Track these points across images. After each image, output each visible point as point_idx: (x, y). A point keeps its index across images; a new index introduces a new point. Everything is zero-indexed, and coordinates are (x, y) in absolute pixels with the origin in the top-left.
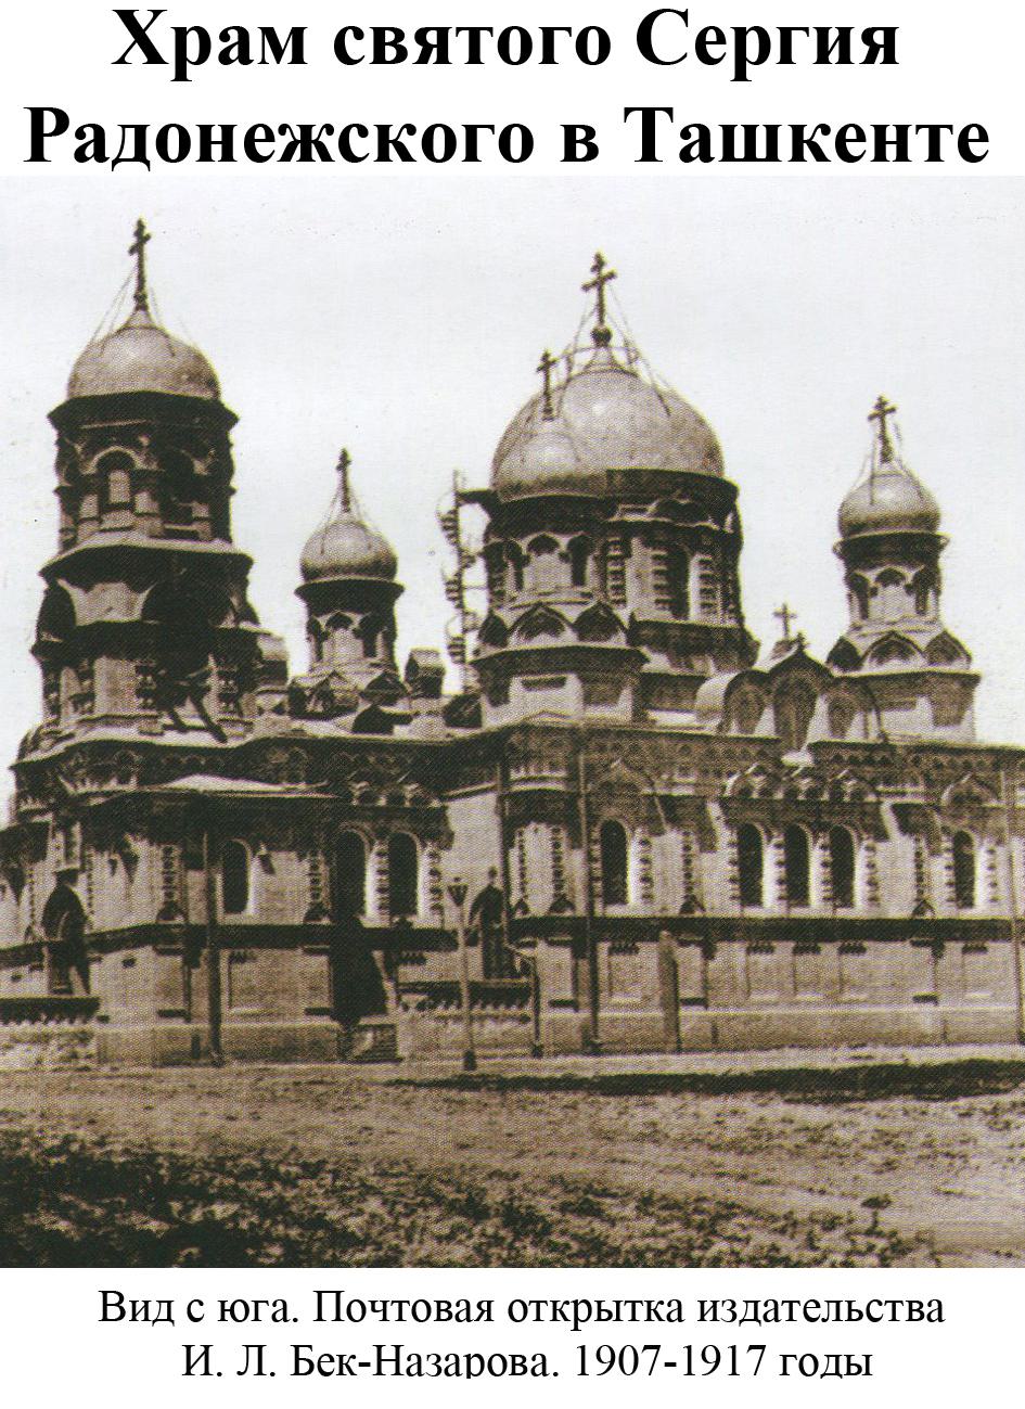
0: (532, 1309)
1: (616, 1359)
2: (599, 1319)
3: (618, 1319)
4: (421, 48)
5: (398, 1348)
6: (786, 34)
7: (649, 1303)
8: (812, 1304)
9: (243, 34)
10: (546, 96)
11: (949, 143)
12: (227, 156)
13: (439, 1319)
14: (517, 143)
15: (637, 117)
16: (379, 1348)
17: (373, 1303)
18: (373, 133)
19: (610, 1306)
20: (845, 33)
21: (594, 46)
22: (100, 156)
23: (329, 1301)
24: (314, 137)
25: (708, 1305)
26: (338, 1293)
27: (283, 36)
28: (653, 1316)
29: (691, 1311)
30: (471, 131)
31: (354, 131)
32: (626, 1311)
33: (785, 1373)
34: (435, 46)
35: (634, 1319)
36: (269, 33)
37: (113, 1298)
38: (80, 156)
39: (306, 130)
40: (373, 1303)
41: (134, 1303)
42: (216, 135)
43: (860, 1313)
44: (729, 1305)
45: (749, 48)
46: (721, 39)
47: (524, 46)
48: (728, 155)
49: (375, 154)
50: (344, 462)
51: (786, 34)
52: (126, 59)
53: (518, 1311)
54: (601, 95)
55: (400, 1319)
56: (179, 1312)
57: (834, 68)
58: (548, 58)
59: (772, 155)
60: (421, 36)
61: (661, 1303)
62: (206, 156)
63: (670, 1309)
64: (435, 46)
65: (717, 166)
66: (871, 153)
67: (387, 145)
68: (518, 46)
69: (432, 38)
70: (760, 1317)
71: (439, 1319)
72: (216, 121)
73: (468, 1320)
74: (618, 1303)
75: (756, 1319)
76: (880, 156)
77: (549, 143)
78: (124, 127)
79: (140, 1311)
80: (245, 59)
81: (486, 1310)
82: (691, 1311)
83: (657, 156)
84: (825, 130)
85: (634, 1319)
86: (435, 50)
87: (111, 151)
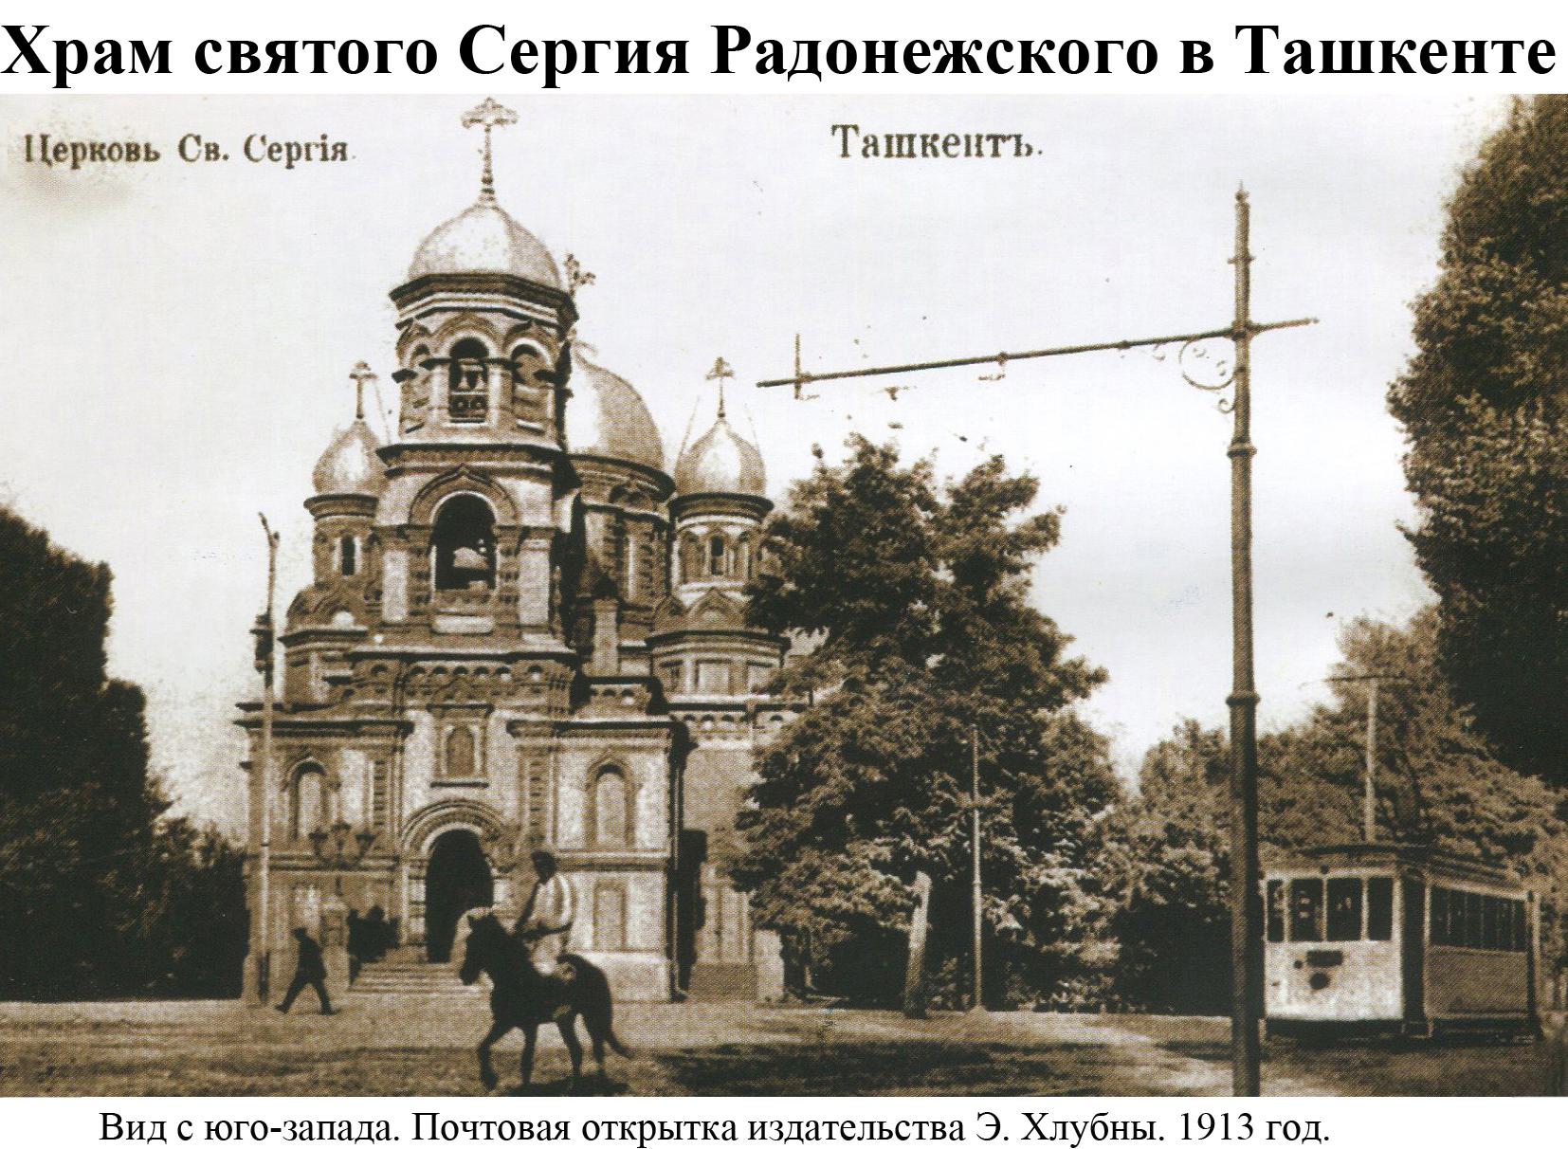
0: (604, 1129)
6: (590, 46)
9: (116, 47)
11: (1520, 57)
15: (1247, 34)
18: (1017, 49)
20: (642, 46)
22: (778, 68)
23: (426, 1122)
25: (757, 1126)
26: (434, 1115)
27: (151, 49)
29: (742, 1131)
31: (1000, 46)
32: (685, 1131)
34: (283, 57)
36: (138, 46)
37: (112, 1120)
38: (761, 68)
39: (957, 45)
46: (533, 51)
48: (1328, 67)
49: (1018, 67)
50: (1316, 321)
51: (590, 46)
53: (591, 1130)
56: (170, 1132)
57: (633, 76)
59: (1366, 67)
60: (271, 48)
64: (283, 57)
65: (1317, 75)
66: (1452, 64)
67: (1029, 58)
69: (281, 50)
72: (880, 37)
76: (1460, 68)
77: (1171, 57)
79: (136, 1131)
80: (117, 68)
81: (564, 1130)
82: (742, 1131)
84: (1412, 45)
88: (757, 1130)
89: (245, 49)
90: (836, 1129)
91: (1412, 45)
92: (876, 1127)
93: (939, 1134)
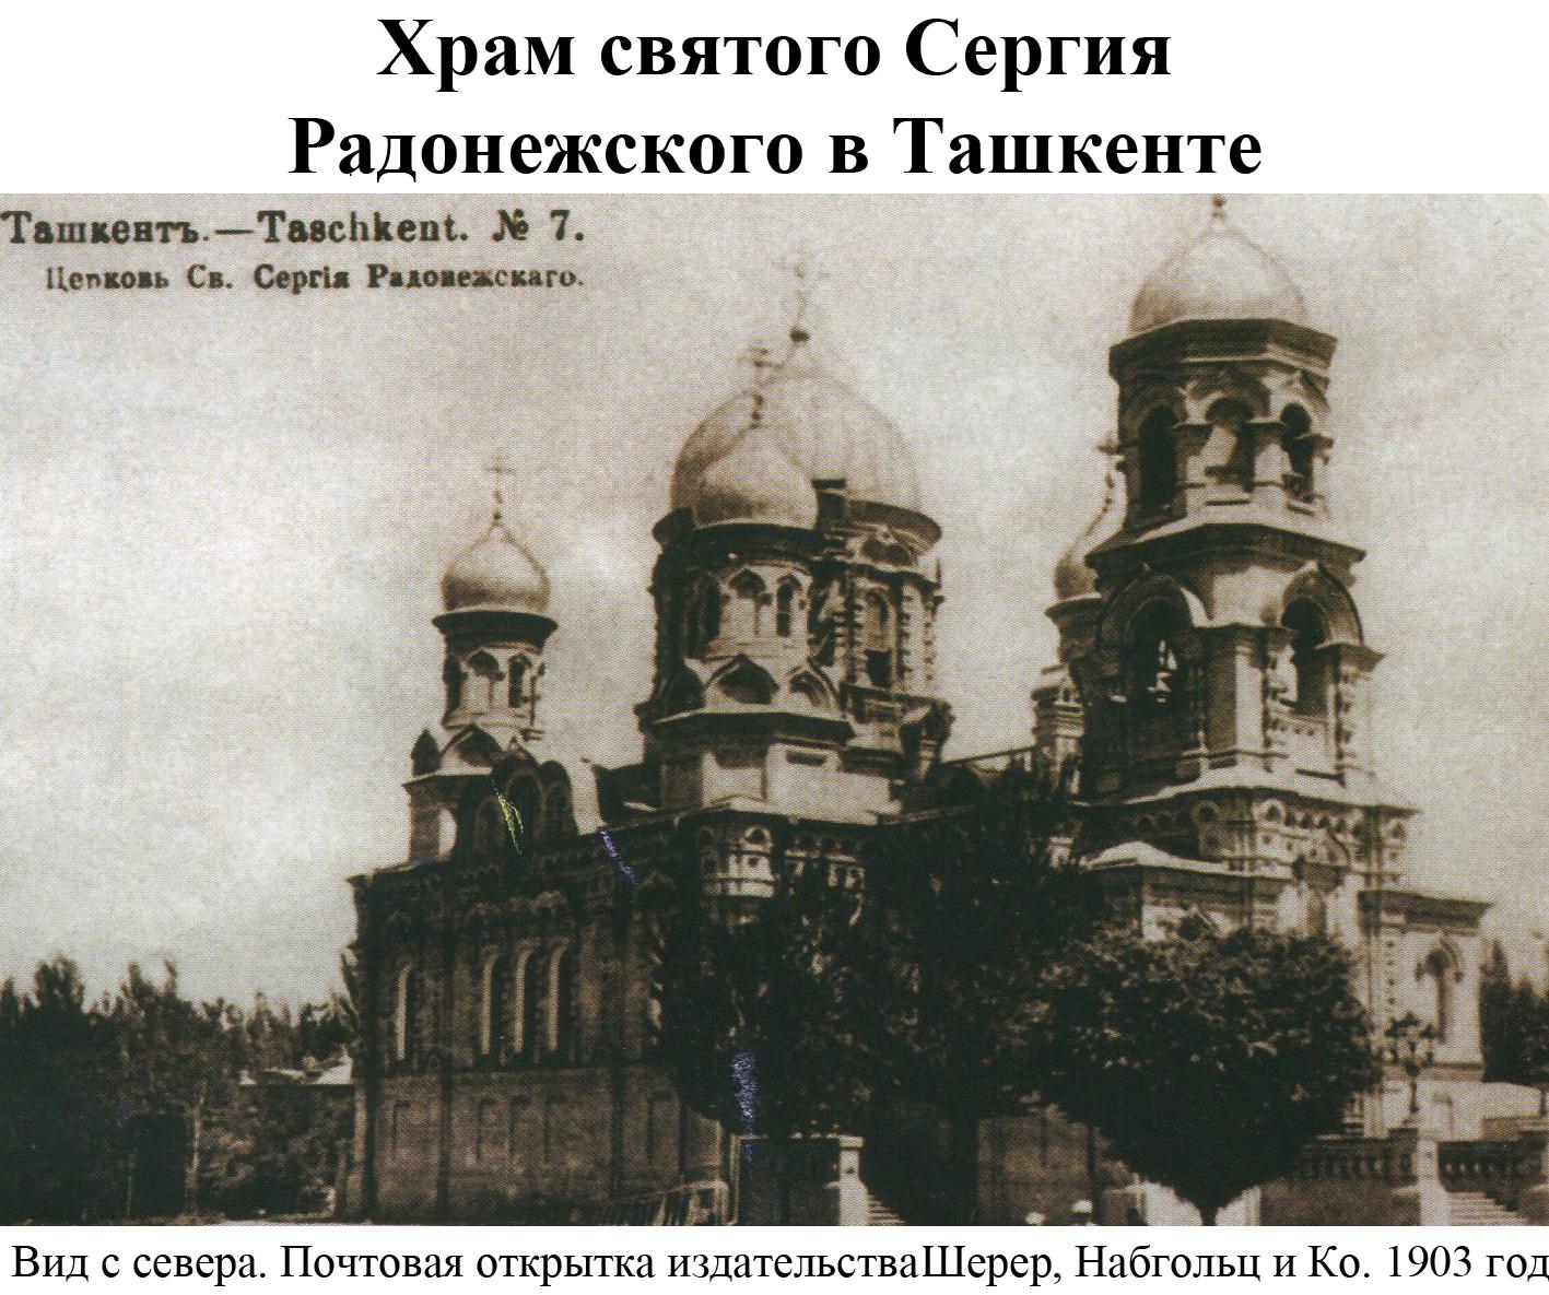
0: (502, 1265)
1: (1429, 1260)
2: (569, 1274)
3: (588, 1274)
4: (1139, 58)
5: (1100, 1249)
6: (1057, 44)
7: (619, 1258)
8: (784, 1259)
9: (510, 45)
10: (814, 107)
11: (1221, 154)
12: (494, 167)
13: (407, 1274)
14: (786, 154)
15: (906, 128)
16: (1082, 1249)
17: (341, 1258)
18: (641, 144)
19: (579, 1261)
20: (1116, 43)
21: (863, 56)
22: (365, 167)
23: (296, 1257)
24: (581, 148)
25: (678, 1261)
26: (306, 1249)
27: (550, 46)
28: (623, 1271)
29: (661, 1266)
30: (740, 142)
31: (621, 142)
32: (596, 1266)
33: (1492, 1274)
34: (702, 56)
35: (604, 1274)
37: (26, 1254)
38: (345, 167)
39: (573, 140)
40: (341, 1258)
41: (47, 1258)
42: (483, 146)
43: (832, 1268)
44: (701, 1260)
45: (1018, 59)
46: (991, 49)
47: (794, 56)
48: (999, 166)
49: (642, 165)
51: (1057, 44)
52: (392, 69)
53: (487, 1266)
54: (871, 105)
55: (369, 1274)
56: (93, 1267)
57: (1105, 79)
58: (817, 68)
59: (1043, 166)
61: (632, 1258)
62: (472, 167)
63: (640, 1264)
64: (702, 56)
66: (1142, 164)
68: (786, 56)
69: (700, 48)
70: (731, 1272)
71: (407, 1274)
72: (483, 131)
73: (438, 1275)
74: (588, 1258)
75: (727, 1274)
76: (1152, 167)
77: (818, 154)
78: (389, 138)
79: (53, 1266)
80: (511, 69)
81: (455, 1266)
82: (661, 1266)
83: (927, 167)
84: (1096, 140)
85: (604, 1274)
86: (1153, 60)
87: (376, 162)
88: (679, 1266)
89: (657, 47)
90: (770, 1264)
91: (1096, 140)
92: (816, 1262)
93: (888, 1270)
